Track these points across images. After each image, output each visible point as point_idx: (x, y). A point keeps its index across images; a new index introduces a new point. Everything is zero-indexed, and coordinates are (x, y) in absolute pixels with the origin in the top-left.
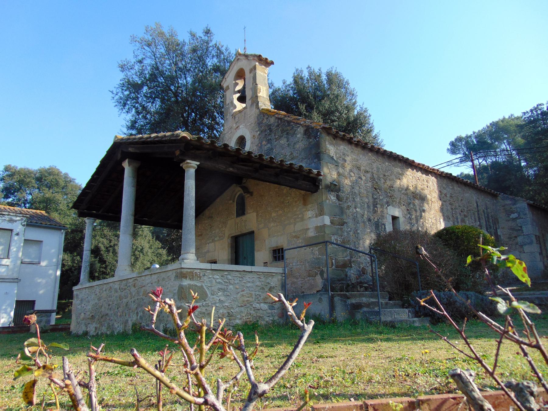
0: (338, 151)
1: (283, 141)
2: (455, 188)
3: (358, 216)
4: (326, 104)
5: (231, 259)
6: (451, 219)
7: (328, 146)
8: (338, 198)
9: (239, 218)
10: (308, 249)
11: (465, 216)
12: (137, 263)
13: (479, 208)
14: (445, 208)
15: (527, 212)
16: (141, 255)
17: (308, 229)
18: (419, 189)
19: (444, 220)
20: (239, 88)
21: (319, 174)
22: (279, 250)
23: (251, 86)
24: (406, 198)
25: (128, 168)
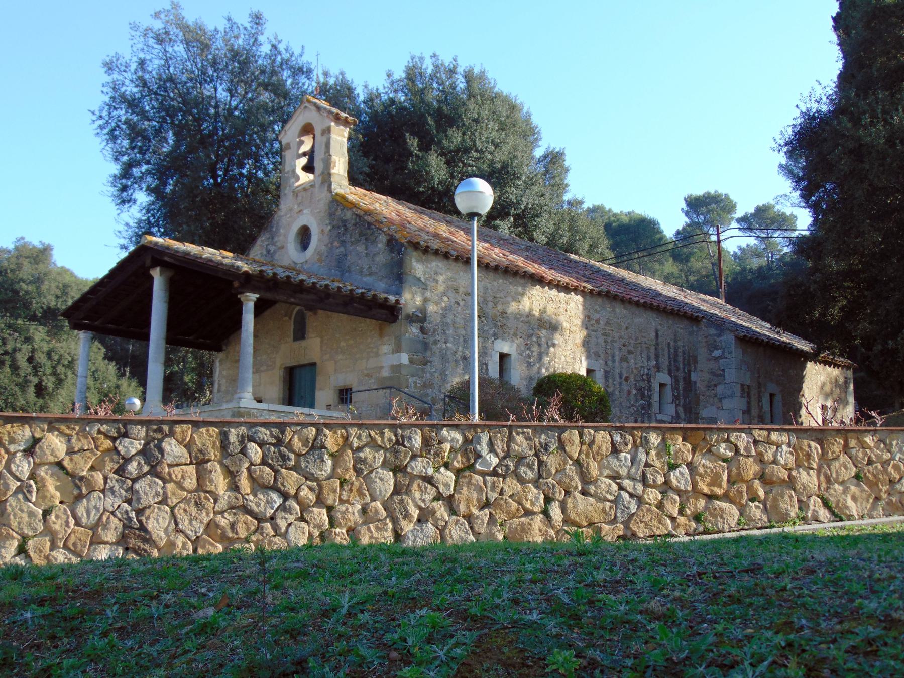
0: (428, 270)
1: (360, 248)
2: (618, 311)
3: (449, 353)
4: (455, 137)
5: (284, 399)
6: (602, 355)
7: (414, 264)
8: (422, 330)
9: (297, 343)
10: (381, 392)
11: (630, 352)
12: (61, 390)
13: (660, 339)
14: (593, 340)
15: (733, 349)
16: (69, 373)
17: (382, 367)
18: (549, 313)
19: (588, 357)
20: (306, 147)
21: (397, 302)
22: (347, 390)
23: (323, 156)
24: (526, 327)
25: (158, 280)
